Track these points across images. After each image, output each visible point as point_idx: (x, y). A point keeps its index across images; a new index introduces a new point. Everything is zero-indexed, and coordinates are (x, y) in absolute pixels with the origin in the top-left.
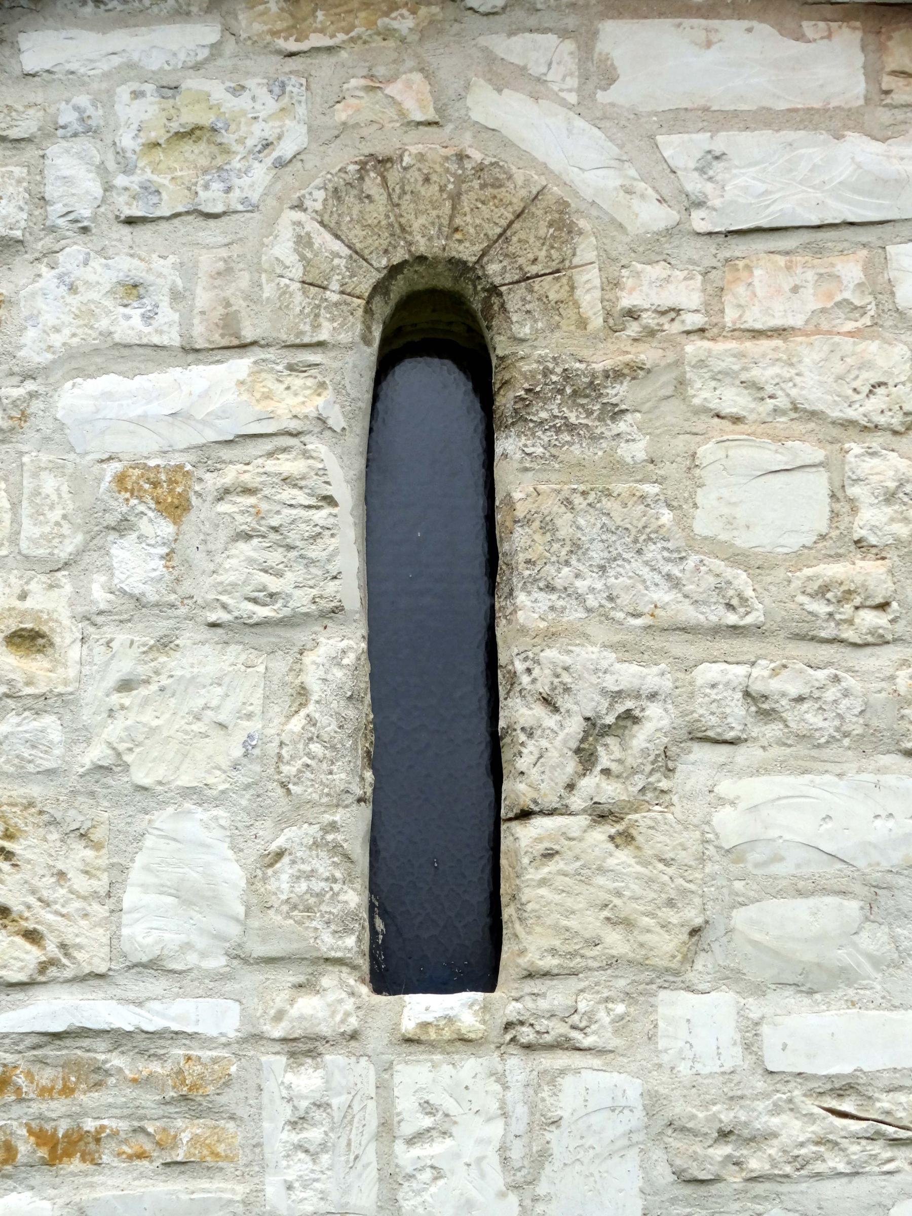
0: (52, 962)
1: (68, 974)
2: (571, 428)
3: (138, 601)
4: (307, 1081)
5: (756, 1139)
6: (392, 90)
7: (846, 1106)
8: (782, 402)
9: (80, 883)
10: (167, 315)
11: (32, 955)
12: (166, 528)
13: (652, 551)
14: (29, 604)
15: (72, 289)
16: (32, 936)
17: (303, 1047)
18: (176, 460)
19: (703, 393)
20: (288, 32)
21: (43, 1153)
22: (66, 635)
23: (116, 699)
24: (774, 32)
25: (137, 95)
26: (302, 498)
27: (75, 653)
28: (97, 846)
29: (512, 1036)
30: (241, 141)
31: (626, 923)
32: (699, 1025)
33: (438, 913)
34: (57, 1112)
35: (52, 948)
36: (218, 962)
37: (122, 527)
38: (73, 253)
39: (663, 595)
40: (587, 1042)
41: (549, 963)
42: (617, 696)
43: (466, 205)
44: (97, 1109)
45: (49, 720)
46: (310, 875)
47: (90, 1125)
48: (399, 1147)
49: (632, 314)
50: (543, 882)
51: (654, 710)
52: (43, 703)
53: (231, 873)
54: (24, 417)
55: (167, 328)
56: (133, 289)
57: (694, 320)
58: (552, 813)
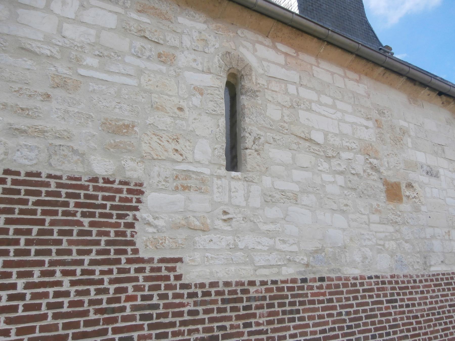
0: (184, 159)
1: (187, 161)
2: (252, 97)
3: (196, 107)
4: (219, 182)
5: (273, 197)
6: (230, 43)
7: (283, 194)
8: (276, 100)
9: (188, 148)
11: (181, 158)
12: (200, 97)
13: (262, 116)
14: (180, 103)
15: (186, 58)
16: (181, 155)
17: (219, 177)
18: (201, 87)
19: (267, 97)
20: (216, 30)
21: (183, 188)
22: (186, 110)
23: (194, 121)
25: (195, 32)
26: (219, 97)
27: (187, 112)
28: (191, 143)
30: (210, 43)
31: (259, 166)
32: (267, 181)
33: (233, 161)
34: (185, 183)
35: (184, 158)
36: (207, 163)
37: (194, 95)
38: (186, 52)
39: (263, 122)
40: (254, 181)
41: (250, 170)
42: (258, 135)
43: (239, 62)
44: (189, 183)
45: (184, 122)
46: (220, 152)
47: (189, 185)
48: (231, 193)
49: (259, 84)
50: (249, 158)
51: (262, 137)
52: (183, 119)
53: (210, 151)
54: (179, 75)
55: (200, 67)
56: (195, 60)
57: (266, 87)
58: (250, 149)
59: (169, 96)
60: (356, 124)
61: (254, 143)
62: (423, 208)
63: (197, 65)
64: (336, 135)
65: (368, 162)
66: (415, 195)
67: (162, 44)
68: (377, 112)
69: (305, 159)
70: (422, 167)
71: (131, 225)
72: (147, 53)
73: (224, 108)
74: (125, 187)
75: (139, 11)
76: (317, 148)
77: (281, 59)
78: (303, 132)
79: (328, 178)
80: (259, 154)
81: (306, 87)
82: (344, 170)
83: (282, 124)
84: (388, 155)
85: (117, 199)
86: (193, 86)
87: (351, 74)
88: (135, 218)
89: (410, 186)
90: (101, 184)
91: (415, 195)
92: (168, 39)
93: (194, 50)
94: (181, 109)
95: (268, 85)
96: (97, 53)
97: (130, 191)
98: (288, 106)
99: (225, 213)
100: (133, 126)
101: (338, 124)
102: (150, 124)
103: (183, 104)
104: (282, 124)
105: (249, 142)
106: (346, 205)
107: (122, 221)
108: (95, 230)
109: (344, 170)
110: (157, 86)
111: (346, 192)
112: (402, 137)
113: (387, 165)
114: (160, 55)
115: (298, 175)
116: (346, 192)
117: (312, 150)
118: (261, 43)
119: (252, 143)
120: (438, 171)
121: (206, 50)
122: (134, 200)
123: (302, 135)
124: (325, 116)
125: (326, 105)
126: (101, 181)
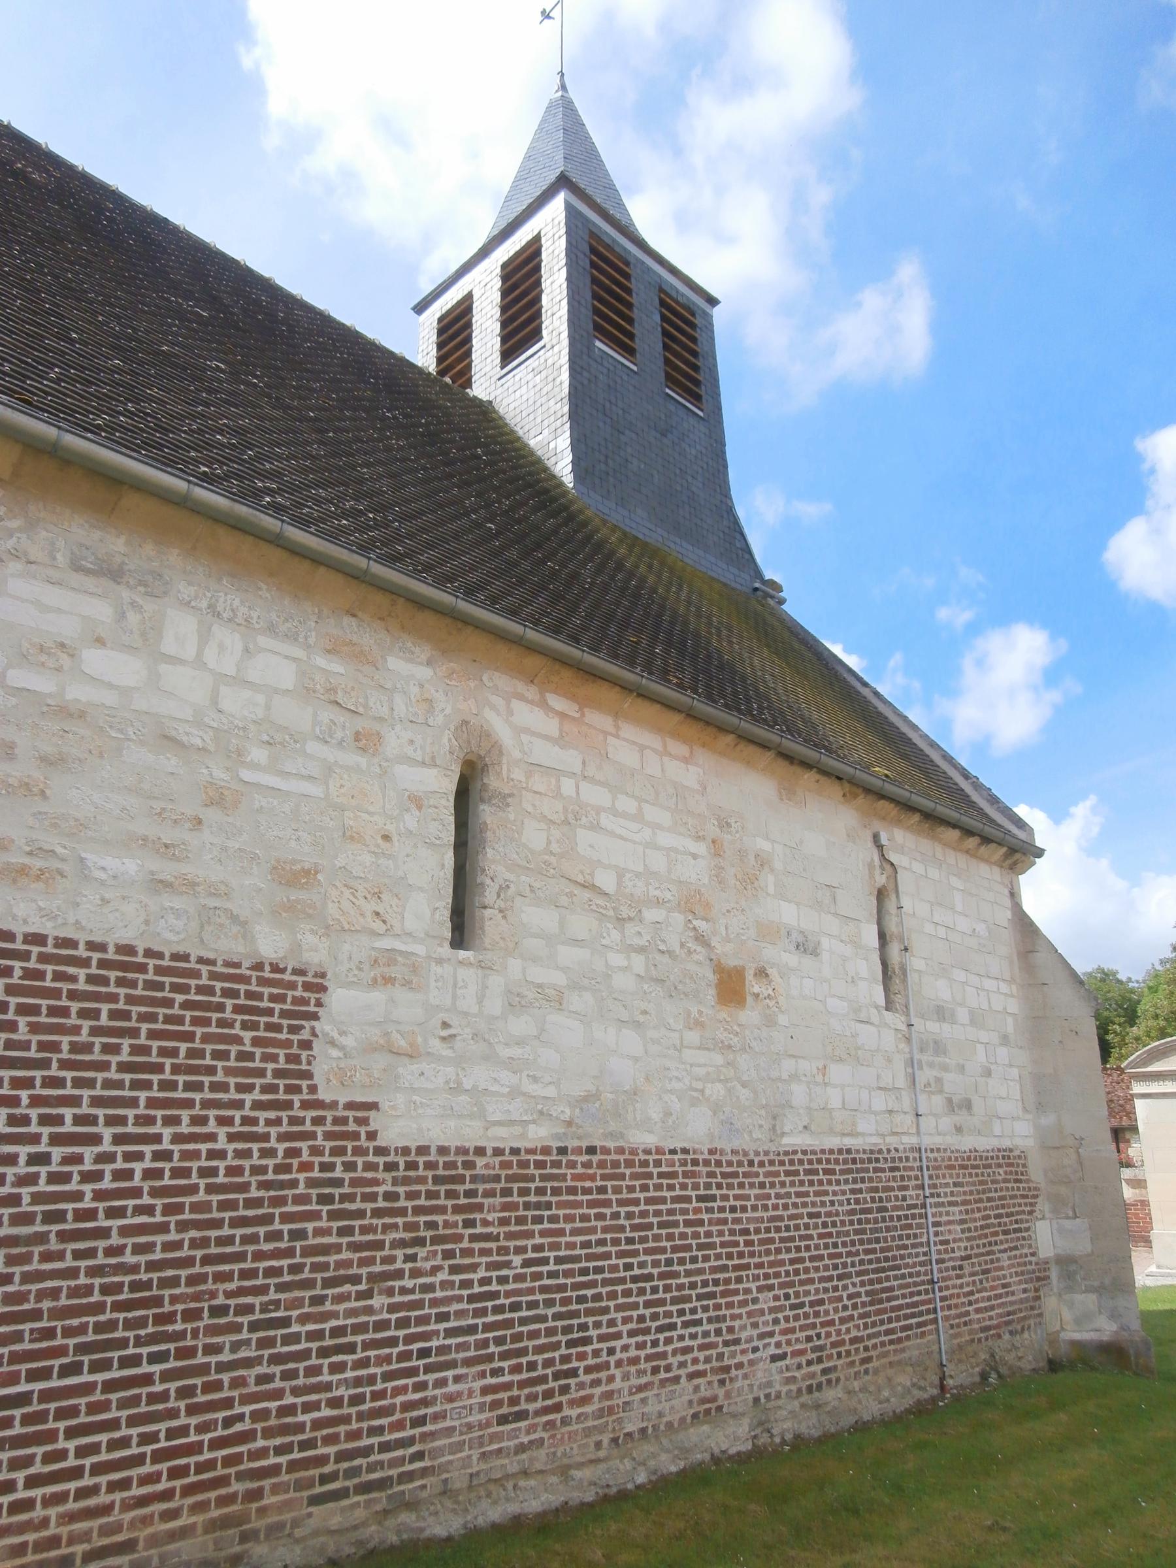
4: (439, 970)
10: (419, 752)
29: (480, 965)
44: (394, 971)
55: (418, 756)
56: (411, 742)
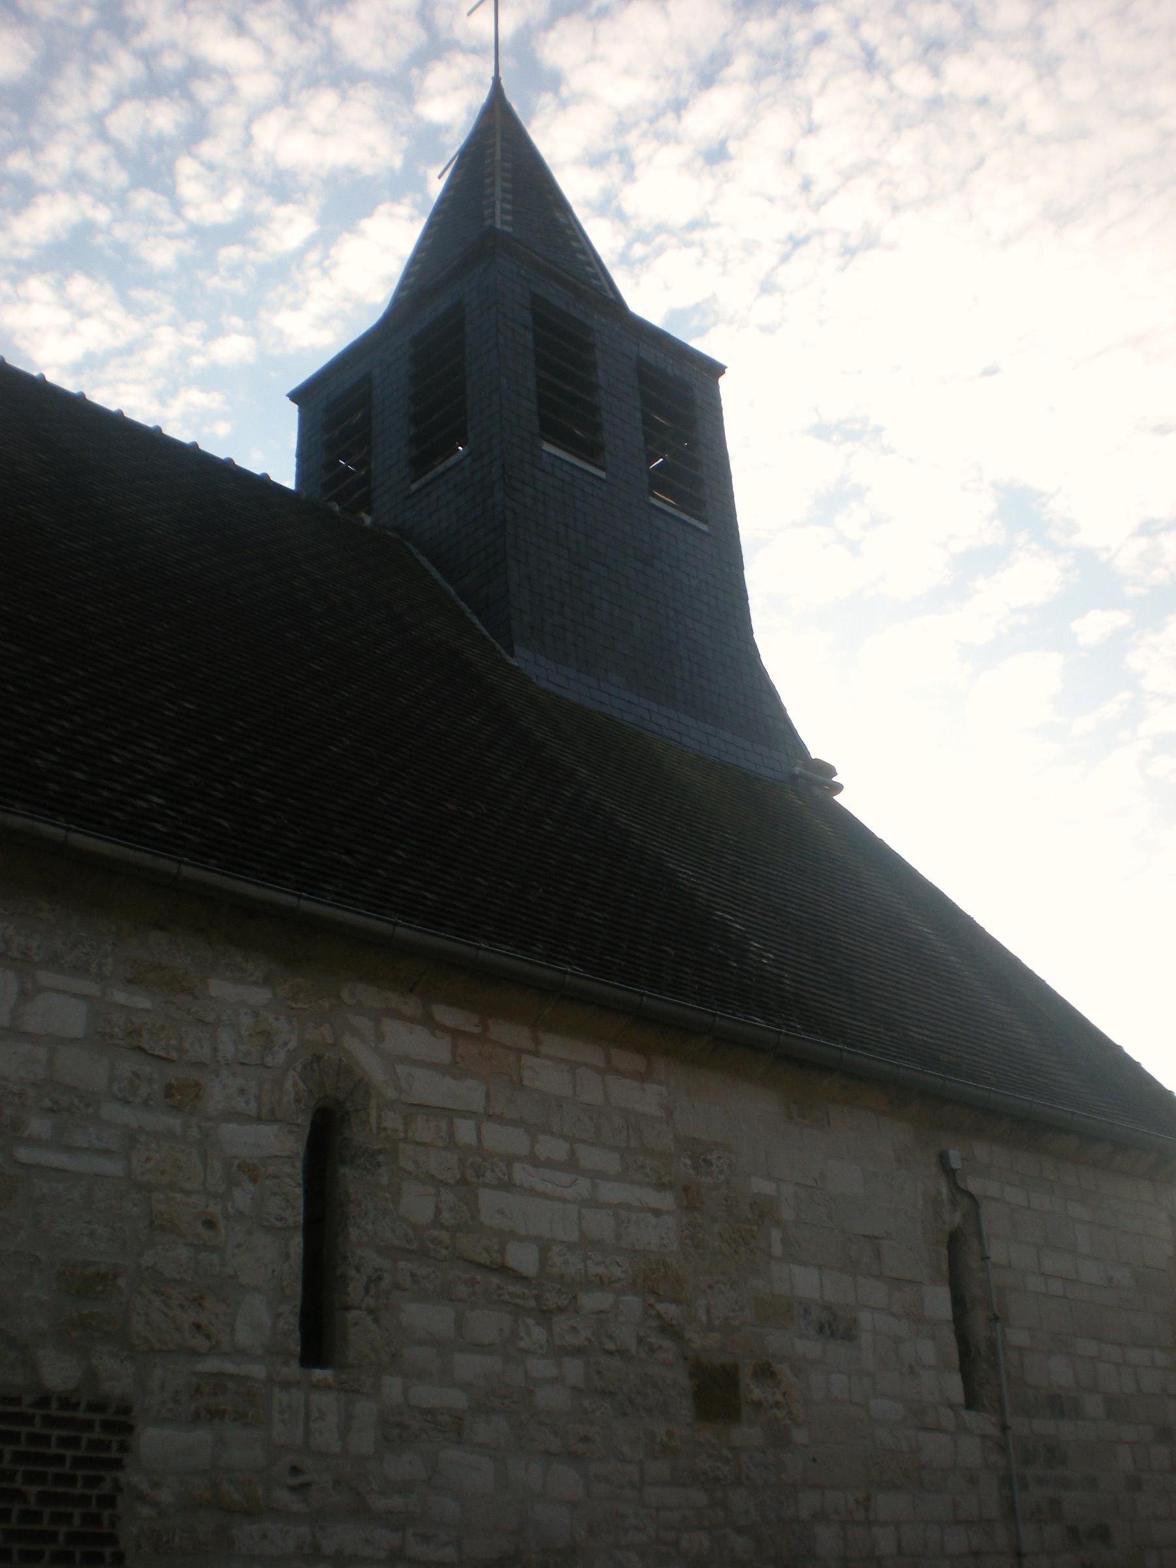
7: (429, 1418)
16: (208, 1337)
24: (128, 415)
42: (377, 1270)
49: (385, 1129)
55: (252, 1110)
56: (242, 1092)
59: (186, 1192)
60: (628, 1206)
61: (367, 1290)
62: (800, 1436)
63: (247, 1102)
64: (571, 1247)
65: (653, 1313)
66: (779, 1397)
67: (173, 1061)
68: (688, 1162)
69: (487, 1324)
70: (806, 1312)
71: (108, 1501)
72: (144, 1091)
73: (302, 1209)
74: (98, 1417)
75: (130, 982)
76: (517, 1289)
77: (441, 1049)
78: (487, 1249)
79: (541, 1367)
80: (376, 1320)
81: (500, 1119)
82: (586, 1343)
83: (435, 1233)
84: (710, 1287)
85: (84, 1444)
86: (236, 1162)
87: (625, 1060)
88: (117, 1487)
89: (765, 1372)
90: (54, 1411)
91: (779, 1397)
92: (187, 1046)
93: (242, 1064)
94: (210, 1224)
95: (406, 1131)
96: (47, 1103)
97: (107, 1426)
98: (452, 1181)
99: (295, 1470)
100: (116, 1276)
101: (579, 1213)
102: (148, 1268)
103: (215, 1209)
104: (435, 1233)
105: (355, 1290)
106: (585, 1439)
107: (94, 1492)
108: (47, 1511)
109: (586, 1343)
110: (163, 1173)
111: (586, 1403)
112: (755, 1228)
113: (704, 1318)
114: (169, 1091)
115: (468, 1366)
116: (586, 1403)
117: (506, 1297)
118: (396, 1015)
119: (363, 1293)
120: (855, 1321)
121: (269, 1060)
122: (115, 1446)
123: (484, 1258)
124: (545, 1196)
125: (550, 1164)
126: (55, 1404)
